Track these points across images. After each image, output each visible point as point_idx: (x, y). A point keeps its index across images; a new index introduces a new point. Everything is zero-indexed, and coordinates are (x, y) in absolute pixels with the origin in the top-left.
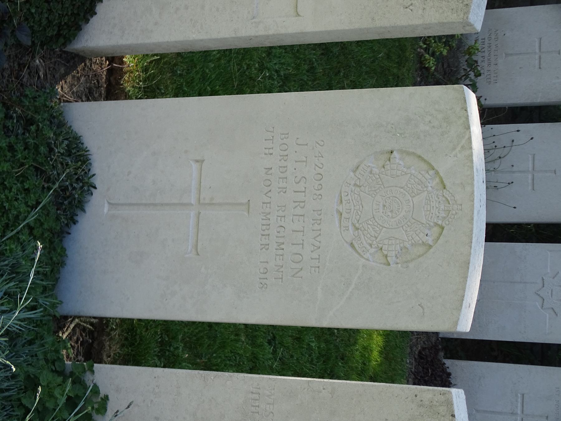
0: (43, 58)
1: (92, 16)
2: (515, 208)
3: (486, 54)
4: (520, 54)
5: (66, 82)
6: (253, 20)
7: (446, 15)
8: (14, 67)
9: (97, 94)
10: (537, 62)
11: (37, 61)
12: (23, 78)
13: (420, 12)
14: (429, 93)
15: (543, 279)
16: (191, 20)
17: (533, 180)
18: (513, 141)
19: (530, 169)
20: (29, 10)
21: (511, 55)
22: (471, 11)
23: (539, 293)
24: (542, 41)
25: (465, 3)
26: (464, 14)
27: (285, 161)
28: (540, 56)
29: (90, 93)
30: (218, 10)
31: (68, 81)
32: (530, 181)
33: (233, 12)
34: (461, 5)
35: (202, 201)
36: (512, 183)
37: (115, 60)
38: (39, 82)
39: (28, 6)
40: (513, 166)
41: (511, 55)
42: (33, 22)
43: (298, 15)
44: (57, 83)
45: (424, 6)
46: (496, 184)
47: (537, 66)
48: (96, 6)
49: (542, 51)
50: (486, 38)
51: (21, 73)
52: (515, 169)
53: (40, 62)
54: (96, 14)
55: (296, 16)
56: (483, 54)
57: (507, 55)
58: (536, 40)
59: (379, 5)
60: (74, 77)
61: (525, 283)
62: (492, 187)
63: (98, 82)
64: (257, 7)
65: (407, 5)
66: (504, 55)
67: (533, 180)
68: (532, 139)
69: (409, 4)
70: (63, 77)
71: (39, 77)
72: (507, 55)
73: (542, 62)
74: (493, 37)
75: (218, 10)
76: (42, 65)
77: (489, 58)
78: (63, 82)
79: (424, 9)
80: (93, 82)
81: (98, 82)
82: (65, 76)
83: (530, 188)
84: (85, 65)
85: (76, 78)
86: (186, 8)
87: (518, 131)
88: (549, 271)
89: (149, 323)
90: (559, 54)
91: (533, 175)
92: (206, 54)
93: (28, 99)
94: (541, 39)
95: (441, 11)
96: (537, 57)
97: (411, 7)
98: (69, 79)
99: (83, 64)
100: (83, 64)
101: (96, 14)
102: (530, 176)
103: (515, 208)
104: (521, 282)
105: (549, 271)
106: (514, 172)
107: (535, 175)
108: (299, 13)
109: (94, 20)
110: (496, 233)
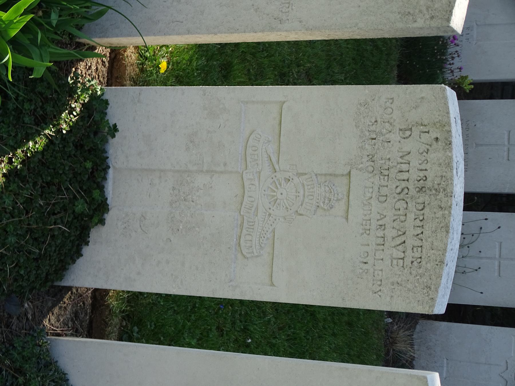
1: (78, 258)
2: (482, 293)
4: (490, 145)
5: (53, 314)
6: (231, 283)
7: (412, 305)
8: (4, 316)
9: (83, 315)
10: (506, 153)
11: (26, 305)
12: (12, 325)
13: (388, 299)
14: (395, 379)
15: (507, 362)
16: (172, 275)
17: (500, 266)
18: (481, 228)
19: (497, 256)
20: (18, 272)
21: (482, 145)
22: (436, 305)
23: (502, 375)
24: (511, 134)
25: (430, 297)
26: (429, 307)
28: (509, 149)
29: (76, 317)
30: (197, 269)
31: (55, 313)
32: (497, 268)
33: (212, 273)
34: (427, 298)
36: (480, 268)
37: (99, 295)
38: (27, 324)
39: (17, 269)
40: (480, 252)
41: (482, 145)
42: (22, 281)
43: (272, 285)
44: (45, 317)
45: (392, 294)
46: (465, 269)
47: (506, 158)
48: (82, 248)
49: (510, 143)
51: (11, 320)
52: (482, 255)
53: (28, 305)
54: (82, 255)
55: (271, 286)
57: (477, 145)
59: (349, 286)
60: (60, 308)
61: (489, 364)
62: (460, 271)
63: (84, 303)
64: (234, 271)
65: (376, 291)
66: (474, 145)
67: (500, 266)
68: (499, 228)
69: (378, 290)
70: (50, 309)
71: (27, 319)
72: (477, 145)
73: (510, 155)
75: (197, 269)
76: (30, 307)
78: (51, 314)
79: (392, 297)
80: (79, 305)
81: (84, 303)
82: (53, 308)
83: (496, 274)
84: (72, 293)
85: (63, 309)
86: (168, 262)
87: (486, 219)
88: (513, 355)
91: (500, 262)
93: (17, 351)
95: (408, 301)
96: (506, 149)
97: (379, 293)
98: (56, 310)
99: (70, 292)
100: (70, 292)
101: (82, 255)
102: (497, 263)
103: (482, 293)
104: (486, 364)
105: (513, 355)
106: (481, 258)
107: (502, 262)
108: (274, 283)
109: (80, 261)
110: (474, 202)
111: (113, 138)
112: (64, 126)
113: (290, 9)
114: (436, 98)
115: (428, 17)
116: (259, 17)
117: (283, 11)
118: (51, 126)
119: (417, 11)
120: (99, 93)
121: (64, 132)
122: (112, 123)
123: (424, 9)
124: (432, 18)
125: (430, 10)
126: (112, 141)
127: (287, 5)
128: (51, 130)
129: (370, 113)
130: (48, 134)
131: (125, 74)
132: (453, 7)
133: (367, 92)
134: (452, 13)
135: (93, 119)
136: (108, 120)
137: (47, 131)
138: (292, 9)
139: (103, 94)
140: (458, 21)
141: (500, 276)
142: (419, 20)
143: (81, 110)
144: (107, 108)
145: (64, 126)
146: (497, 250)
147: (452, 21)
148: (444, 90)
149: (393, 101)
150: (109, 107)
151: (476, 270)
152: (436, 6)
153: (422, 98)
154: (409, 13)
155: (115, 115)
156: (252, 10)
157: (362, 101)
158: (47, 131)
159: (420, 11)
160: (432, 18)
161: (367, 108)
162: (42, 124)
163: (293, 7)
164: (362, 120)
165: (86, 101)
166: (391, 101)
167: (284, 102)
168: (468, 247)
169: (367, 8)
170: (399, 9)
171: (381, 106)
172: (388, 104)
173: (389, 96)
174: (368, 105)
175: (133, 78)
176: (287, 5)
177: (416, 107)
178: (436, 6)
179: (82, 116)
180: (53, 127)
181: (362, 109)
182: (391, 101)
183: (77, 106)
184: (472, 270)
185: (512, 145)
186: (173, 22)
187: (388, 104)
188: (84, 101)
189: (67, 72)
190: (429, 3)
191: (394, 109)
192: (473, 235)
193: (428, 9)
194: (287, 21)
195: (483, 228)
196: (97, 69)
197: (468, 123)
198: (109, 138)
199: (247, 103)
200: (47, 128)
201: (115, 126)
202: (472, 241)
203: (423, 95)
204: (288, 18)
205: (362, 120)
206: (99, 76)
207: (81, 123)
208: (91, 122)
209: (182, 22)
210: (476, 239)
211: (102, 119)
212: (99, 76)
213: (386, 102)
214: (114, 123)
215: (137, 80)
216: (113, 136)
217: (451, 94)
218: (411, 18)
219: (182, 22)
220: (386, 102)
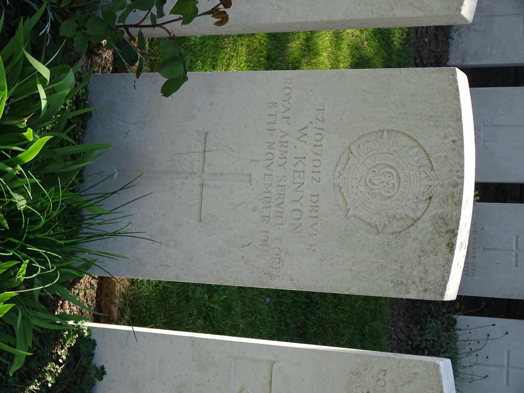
10: (514, 259)
18: (489, 335)
19: (505, 365)
21: (489, 249)
28: (517, 254)
32: (505, 376)
36: (487, 376)
41: (489, 249)
47: (514, 264)
58: (514, 237)
66: (482, 249)
72: (484, 249)
73: (518, 261)
83: (505, 383)
87: (494, 325)
96: (514, 254)
102: (505, 372)
106: (489, 366)
107: (510, 370)
111: (100, 380)
112: (49, 379)
113: (281, 265)
114: (429, 375)
115: (421, 289)
116: (249, 270)
117: (274, 266)
118: (36, 381)
119: (410, 281)
120: (86, 334)
121: (50, 385)
122: (99, 366)
123: (417, 280)
124: (426, 290)
125: (423, 282)
126: (99, 384)
127: (278, 261)
128: (36, 385)
129: (362, 383)
130: (34, 389)
131: (115, 291)
132: (447, 282)
133: (359, 360)
134: (446, 288)
135: (80, 363)
136: (95, 365)
137: (32, 387)
138: (283, 266)
139: (89, 336)
140: (468, 11)
141: (508, 385)
142: (412, 291)
143: (67, 356)
144: (94, 349)
145: (49, 379)
146: (505, 358)
147: (446, 295)
148: (454, 74)
149: (386, 373)
150: (97, 348)
151: (485, 377)
152: (430, 279)
153: (416, 373)
154: (402, 282)
155: (102, 357)
156: (242, 262)
157: (354, 370)
158: (32, 387)
159: (414, 282)
160: (426, 290)
161: (358, 378)
162: (27, 380)
163: (284, 264)
164: (354, 389)
165: (73, 345)
166: (383, 373)
167: (274, 362)
168: (477, 355)
169: (359, 273)
170: (392, 278)
171: (373, 377)
172: (380, 376)
173: (381, 368)
174: (361, 374)
175: (123, 293)
176: (278, 261)
177: (409, 383)
178: (430, 279)
179: (68, 363)
180: (38, 382)
181: (354, 378)
182: (383, 373)
183: (63, 353)
184: (480, 378)
185: (520, 250)
186: (161, 266)
187: (380, 376)
188: (71, 345)
189: (54, 307)
190: (422, 275)
191: (387, 381)
192: (479, 342)
193: (421, 280)
194: (278, 278)
195: (490, 335)
196: (85, 294)
197: (475, 226)
198: (97, 381)
199: (237, 358)
200: (32, 382)
201: (103, 368)
202: (479, 348)
203: (416, 370)
204: (279, 274)
205: (354, 389)
206: (87, 300)
207: (67, 372)
208: (78, 368)
209: (171, 267)
210: (484, 347)
211: (90, 362)
212: (87, 300)
213: (379, 373)
214: (101, 365)
215: (127, 294)
216: (101, 379)
217: (462, 78)
218: (404, 288)
219: (171, 267)
220: (379, 373)
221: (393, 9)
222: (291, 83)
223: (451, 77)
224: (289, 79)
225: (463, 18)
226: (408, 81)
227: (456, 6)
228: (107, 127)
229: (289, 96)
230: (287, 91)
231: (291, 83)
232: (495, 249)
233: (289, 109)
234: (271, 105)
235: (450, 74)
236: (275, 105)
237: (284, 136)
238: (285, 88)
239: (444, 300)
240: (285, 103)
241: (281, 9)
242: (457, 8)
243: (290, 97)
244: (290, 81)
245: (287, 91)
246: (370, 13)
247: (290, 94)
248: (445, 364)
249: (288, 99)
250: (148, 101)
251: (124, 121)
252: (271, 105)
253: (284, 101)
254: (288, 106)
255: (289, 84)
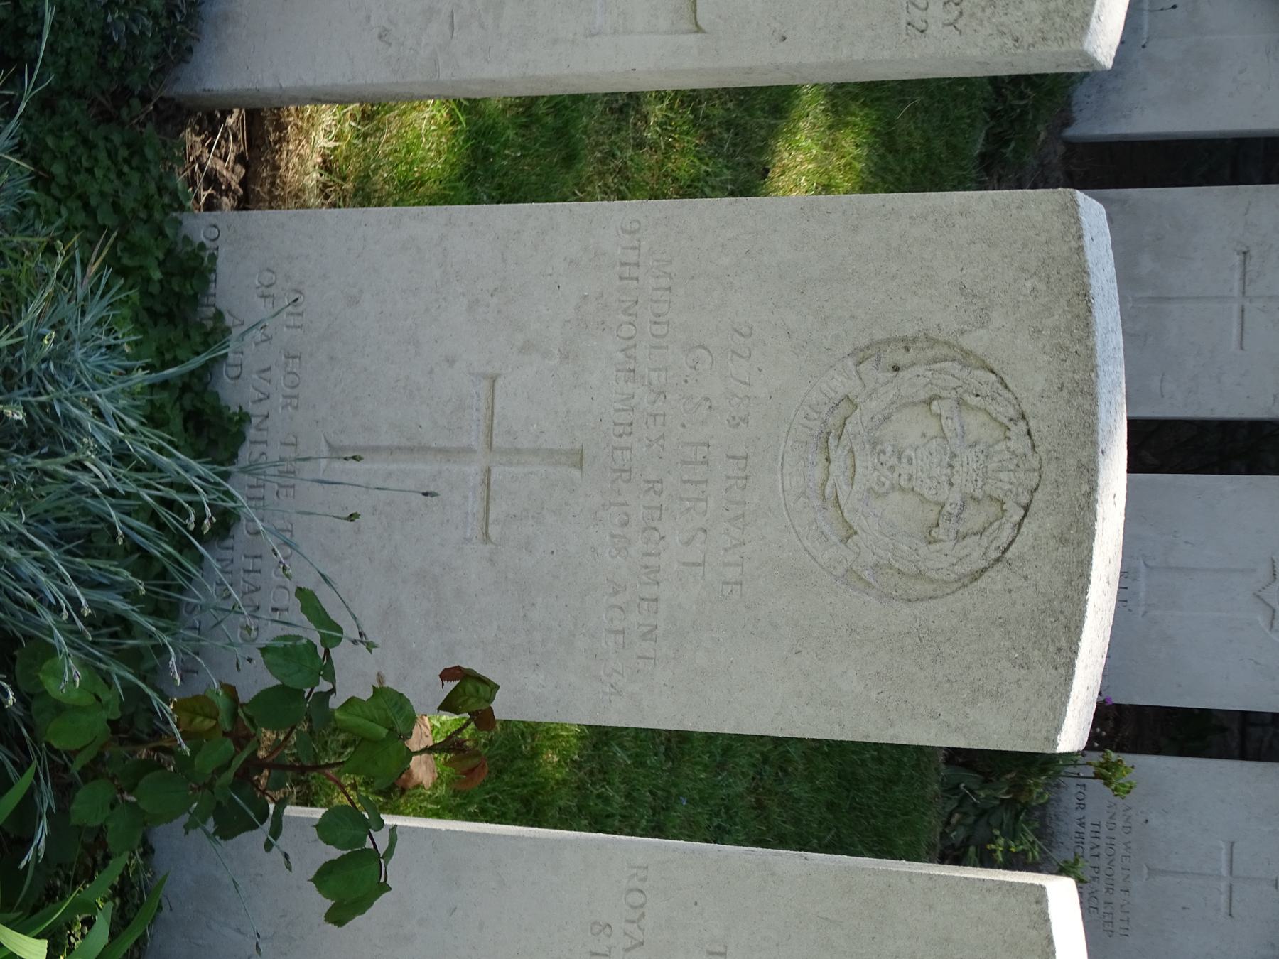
0: (19, 422)
3: (1103, 862)
10: (1224, 899)
21: (1164, 872)
27: (594, 923)
28: (1231, 886)
35: (497, 442)
41: (1164, 872)
47: (1224, 909)
50: (1103, 825)
56: (1096, 862)
57: (1152, 872)
58: (1223, 845)
66: (1145, 871)
72: (1152, 872)
74: (1120, 823)
77: (1109, 872)
89: (503, 196)
90: (580, 466)
92: (1111, 143)
94: (1232, 844)
96: (1223, 886)
140: (1105, 38)
221: (892, 723)
222: (645, 879)
223: (1034, 906)
224: (639, 868)
225: (1089, 59)
226: (931, 907)
227: (1044, 732)
228: (200, 942)
229: (639, 912)
230: (636, 898)
231: (645, 879)
232: (1176, 873)
233: (642, 943)
234: (597, 928)
235: (1032, 899)
236: (608, 930)
237: (633, 947)
238: (631, 890)
239: (1060, 749)
240: (631, 928)
241: (620, 693)
242: (1047, 739)
243: (643, 915)
244: (642, 874)
245: (636, 898)
246: (836, 727)
247: (642, 906)
248: (1062, 895)
249: (639, 920)
250: (299, 888)
251: (238, 930)
252: (597, 928)
253: (628, 921)
254: (639, 935)
255: (641, 880)
